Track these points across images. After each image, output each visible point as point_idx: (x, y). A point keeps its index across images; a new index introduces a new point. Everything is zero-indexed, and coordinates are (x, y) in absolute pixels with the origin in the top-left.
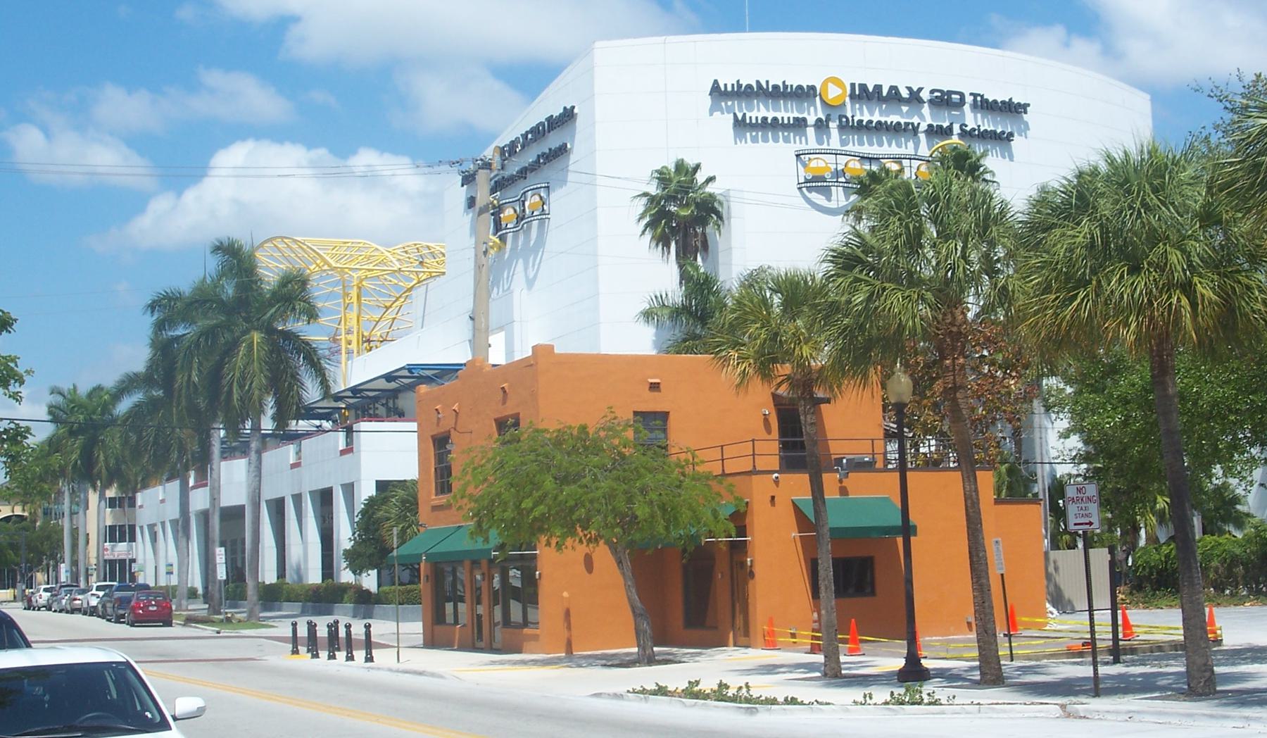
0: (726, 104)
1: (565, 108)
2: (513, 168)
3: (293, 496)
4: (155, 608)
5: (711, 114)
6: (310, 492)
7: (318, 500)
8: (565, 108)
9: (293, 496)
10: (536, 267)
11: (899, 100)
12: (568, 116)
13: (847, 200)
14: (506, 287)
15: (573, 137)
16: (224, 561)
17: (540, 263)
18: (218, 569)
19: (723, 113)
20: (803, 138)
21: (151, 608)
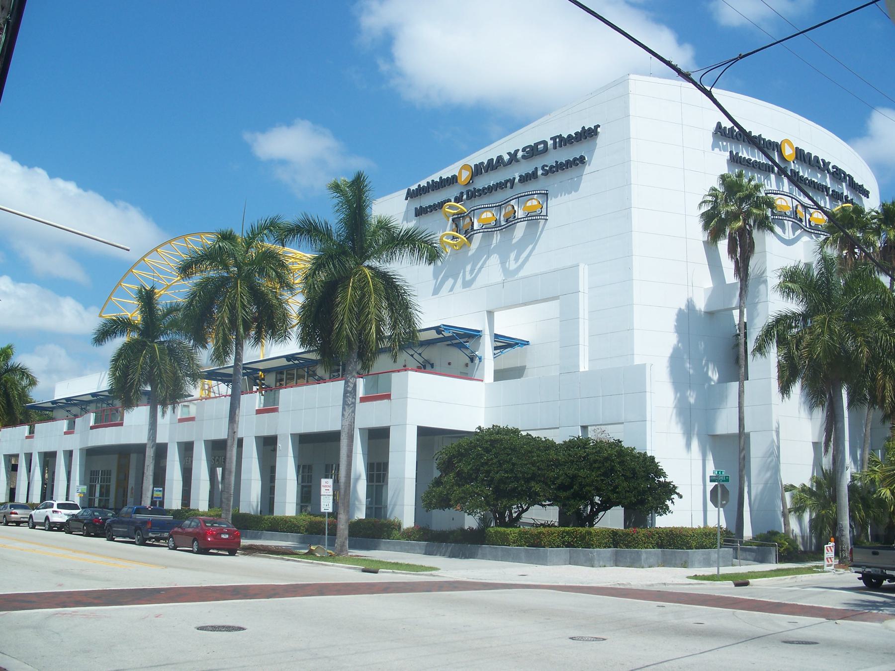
0: (722, 144)
1: (583, 128)
2: (482, 182)
3: (179, 444)
4: (227, 536)
5: (713, 150)
6: (63, 451)
7: (43, 456)
8: (583, 128)
9: (179, 444)
10: (521, 261)
11: (331, 257)
12: (589, 134)
13: (794, 235)
14: (468, 277)
15: (592, 152)
16: (331, 493)
17: (481, 268)
18: (322, 500)
19: (720, 150)
20: (769, 182)
21: (223, 536)
